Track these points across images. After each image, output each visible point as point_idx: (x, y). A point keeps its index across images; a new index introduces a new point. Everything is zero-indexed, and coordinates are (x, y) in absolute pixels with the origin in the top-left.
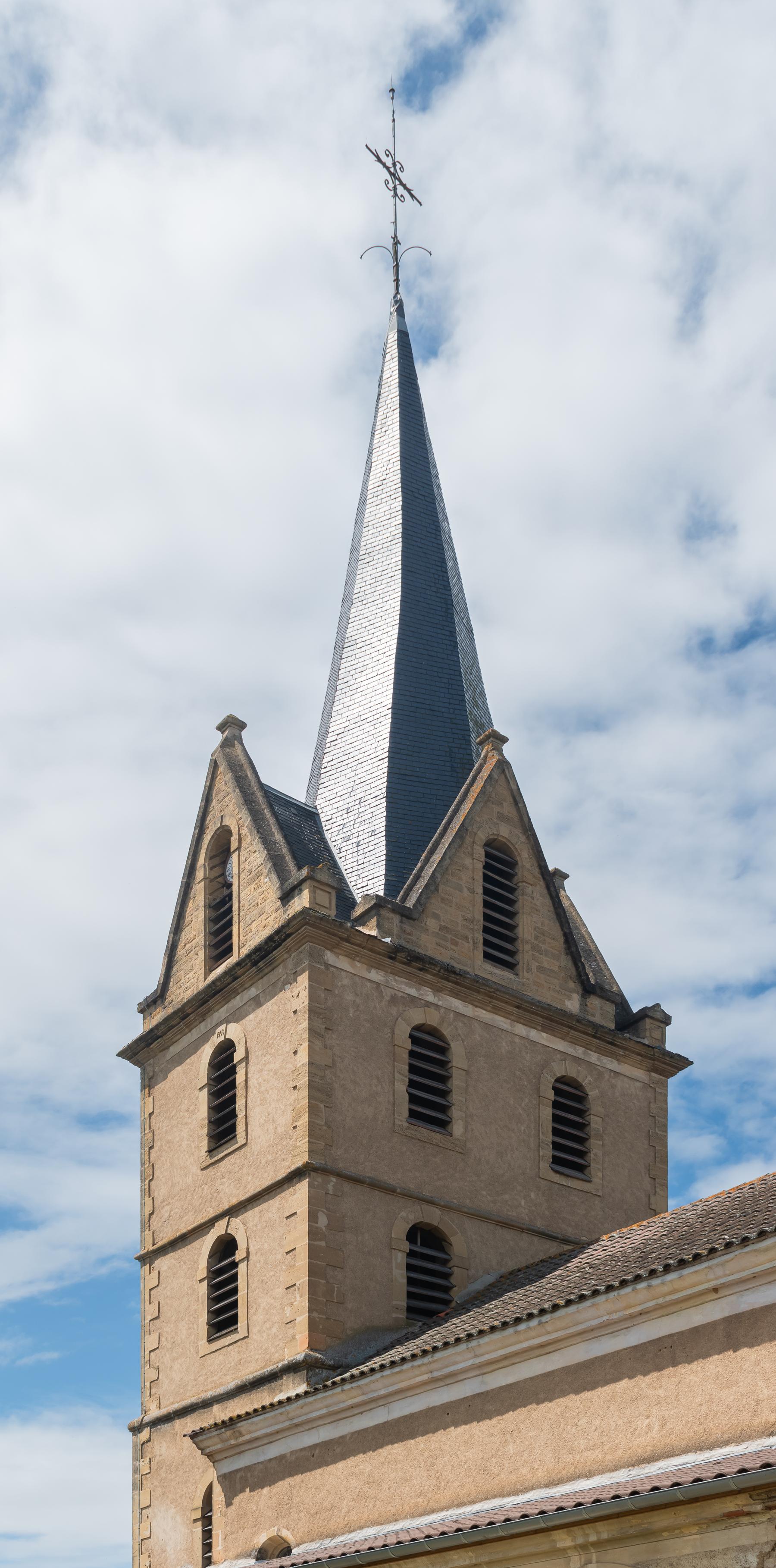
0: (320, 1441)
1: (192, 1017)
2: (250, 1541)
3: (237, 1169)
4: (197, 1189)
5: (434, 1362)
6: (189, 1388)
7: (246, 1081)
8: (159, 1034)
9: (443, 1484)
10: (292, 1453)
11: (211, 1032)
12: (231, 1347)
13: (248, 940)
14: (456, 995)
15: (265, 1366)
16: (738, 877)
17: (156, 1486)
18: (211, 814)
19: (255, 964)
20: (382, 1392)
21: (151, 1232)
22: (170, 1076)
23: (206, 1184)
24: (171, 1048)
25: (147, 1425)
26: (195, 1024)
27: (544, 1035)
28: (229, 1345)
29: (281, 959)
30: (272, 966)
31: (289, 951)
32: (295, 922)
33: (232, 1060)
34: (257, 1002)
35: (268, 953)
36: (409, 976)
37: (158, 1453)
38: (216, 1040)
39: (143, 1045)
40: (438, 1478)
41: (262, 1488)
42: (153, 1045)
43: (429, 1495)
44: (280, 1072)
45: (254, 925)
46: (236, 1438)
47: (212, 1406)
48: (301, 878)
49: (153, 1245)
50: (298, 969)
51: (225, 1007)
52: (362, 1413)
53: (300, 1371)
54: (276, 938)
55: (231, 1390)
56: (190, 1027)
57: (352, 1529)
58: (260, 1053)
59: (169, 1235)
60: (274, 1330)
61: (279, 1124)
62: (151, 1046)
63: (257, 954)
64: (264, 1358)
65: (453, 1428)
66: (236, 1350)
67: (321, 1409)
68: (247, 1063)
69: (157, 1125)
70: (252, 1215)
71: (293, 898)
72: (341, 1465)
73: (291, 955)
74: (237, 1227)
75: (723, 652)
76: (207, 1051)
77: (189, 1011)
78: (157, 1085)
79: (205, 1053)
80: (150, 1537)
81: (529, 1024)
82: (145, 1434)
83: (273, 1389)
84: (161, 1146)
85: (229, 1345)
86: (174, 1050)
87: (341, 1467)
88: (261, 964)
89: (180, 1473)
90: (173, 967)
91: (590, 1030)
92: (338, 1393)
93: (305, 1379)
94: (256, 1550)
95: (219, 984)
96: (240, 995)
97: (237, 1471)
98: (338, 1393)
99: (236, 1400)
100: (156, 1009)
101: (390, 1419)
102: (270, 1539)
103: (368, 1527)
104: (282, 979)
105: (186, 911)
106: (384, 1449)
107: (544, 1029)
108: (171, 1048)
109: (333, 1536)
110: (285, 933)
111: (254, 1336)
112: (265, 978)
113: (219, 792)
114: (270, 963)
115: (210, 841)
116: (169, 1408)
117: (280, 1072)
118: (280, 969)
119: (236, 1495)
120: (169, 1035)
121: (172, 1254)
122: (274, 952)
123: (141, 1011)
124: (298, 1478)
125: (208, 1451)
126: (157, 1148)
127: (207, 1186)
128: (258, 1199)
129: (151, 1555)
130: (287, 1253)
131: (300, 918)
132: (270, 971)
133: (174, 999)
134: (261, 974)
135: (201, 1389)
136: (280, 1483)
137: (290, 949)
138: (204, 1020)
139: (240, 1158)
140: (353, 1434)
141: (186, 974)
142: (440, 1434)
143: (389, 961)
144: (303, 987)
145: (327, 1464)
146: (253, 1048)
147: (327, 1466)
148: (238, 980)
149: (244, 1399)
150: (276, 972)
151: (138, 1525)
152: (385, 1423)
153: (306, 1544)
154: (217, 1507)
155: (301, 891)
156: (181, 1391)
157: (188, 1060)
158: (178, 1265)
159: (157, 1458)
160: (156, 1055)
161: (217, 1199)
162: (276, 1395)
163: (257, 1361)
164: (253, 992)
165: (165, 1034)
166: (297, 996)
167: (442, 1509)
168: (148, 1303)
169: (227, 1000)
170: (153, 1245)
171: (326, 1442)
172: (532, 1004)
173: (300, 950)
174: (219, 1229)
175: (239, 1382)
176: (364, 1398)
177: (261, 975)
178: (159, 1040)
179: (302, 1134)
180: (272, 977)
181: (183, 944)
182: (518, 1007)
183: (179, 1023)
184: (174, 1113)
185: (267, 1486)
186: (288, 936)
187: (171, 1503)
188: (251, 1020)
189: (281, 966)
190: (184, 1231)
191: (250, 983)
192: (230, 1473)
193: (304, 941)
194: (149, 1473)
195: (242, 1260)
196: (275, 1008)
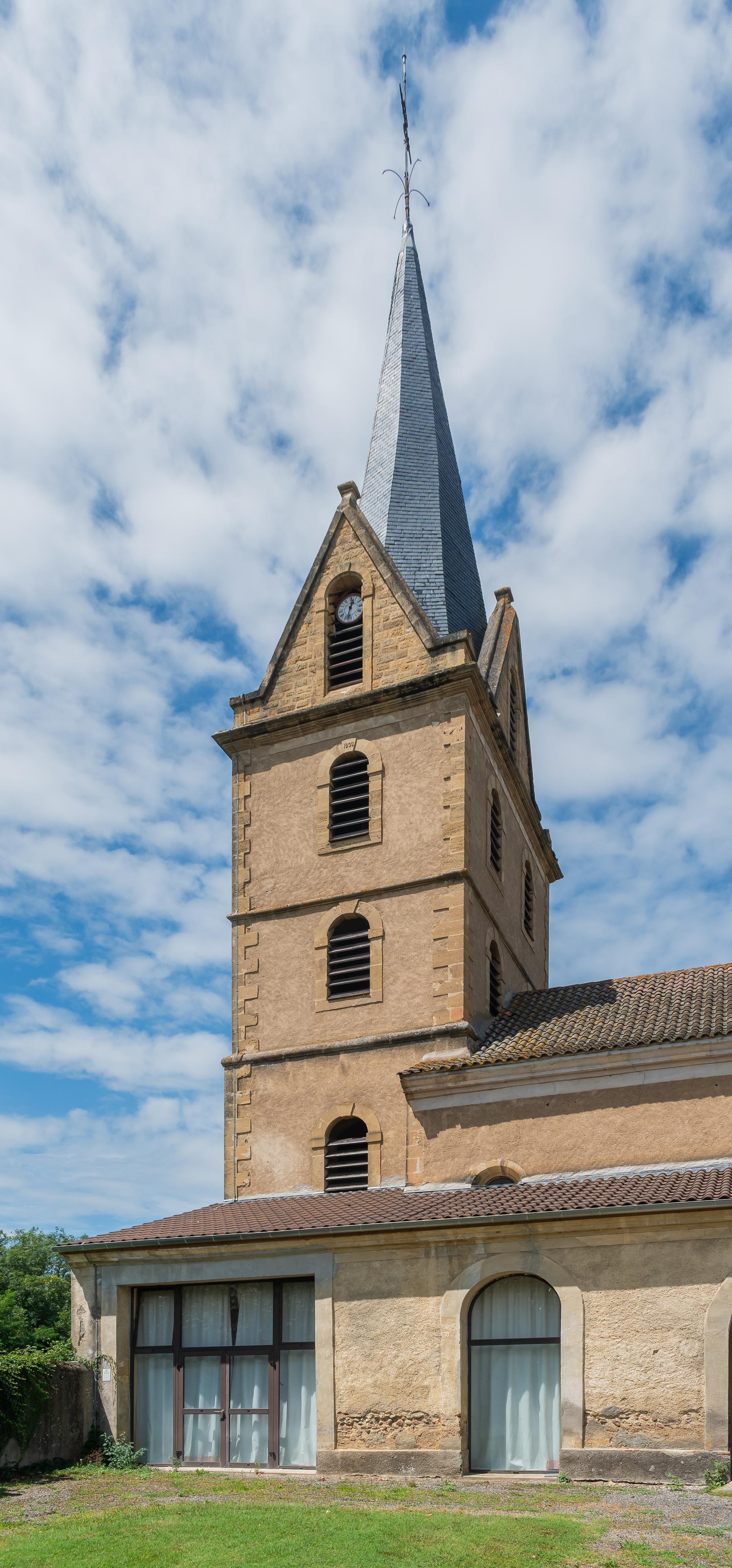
0: (557, 1093)
1: (313, 723)
2: (464, 1168)
3: (368, 862)
4: (312, 871)
5: (722, 1043)
6: (301, 1037)
7: (382, 790)
8: (268, 729)
9: (711, 1138)
10: (519, 1100)
11: (338, 741)
12: (358, 1008)
13: (384, 674)
15: (406, 1029)
17: (259, 1116)
18: (333, 557)
19: (402, 695)
20: (650, 1061)
21: (248, 898)
22: (275, 769)
23: (325, 868)
24: (276, 745)
25: (247, 1062)
26: (312, 730)
28: (356, 1006)
29: (429, 700)
30: (419, 702)
31: (442, 694)
32: (463, 672)
33: (366, 769)
34: (396, 729)
35: (420, 690)
37: (262, 1087)
38: (343, 748)
39: (247, 734)
40: (706, 1133)
41: (479, 1126)
42: (257, 737)
43: (695, 1146)
44: (426, 791)
45: (392, 664)
46: (456, 1082)
47: (339, 1054)
48: (459, 638)
49: (250, 910)
50: (452, 712)
51: (353, 724)
52: (611, 1076)
53: (459, 1037)
54: (437, 679)
55: (368, 1043)
56: (305, 732)
57: (600, 1166)
58: (400, 771)
59: (272, 904)
60: (417, 1000)
61: (425, 834)
62: (255, 738)
63: (410, 688)
64: (404, 1021)
65: (723, 1096)
66: (367, 1011)
67: (574, 1067)
68: (383, 776)
69: (256, 808)
70: (387, 904)
71: (444, 652)
72: (584, 1115)
73: (442, 698)
74: (366, 909)
75: (111, 605)
76: (328, 758)
77: (311, 718)
78: (255, 773)
79: (325, 758)
80: (250, 1159)
82: (244, 1070)
83: (423, 1048)
84: (261, 826)
85: (356, 1006)
86: (278, 747)
87: (584, 1117)
88: (408, 698)
89: (294, 1107)
90: (278, 676)
92: (603, 1057)
93: (465, 1043)
94: (472, 1177)
95: (357, 702)
96: (374, 718)
97: (442, 1110)
98: (603, 1057)
99: (371, 1052)
100: (253, 707)
101: (646, 1082)
102: (489, 1169)
103: (621, 1166)
104: (429, 716)
105: (298, 632)
106: (639, 1106)
108: (276, 745)
109: (576, 1170)
110: (448, 678)
111: (391, 1000)
112: (406, 711)
113: (343, 542)
114: (418, 699)
115: (332, 581)
116: (281, 1050)
117: (426, 791)
118: (427, 707)
119: (442, 1130)
120: (280, 732)
121: (276, 921)
122: (427, 691)
123: (234, 706)
124: (528, 1122)
125: (408, 1090)
126: (256, 827)
127: (326, 870)
128: (398, 890)
129: (251, 1174)
130: (435, 940)
131: (469, 670)
132: (414, 706)
133: (280, 704)
134: (404, 706)
135: (317, 1039)
136: (505, 1124)
137: (445, 693)
138: (324, 729)
139: (372, 853)
140: (600, 1091)
141: (297, 686)
142: (708, 1100)
144: (459, 727)
145: (567, 1113)
146: (390, 763)
147: (567, 1114)
148: (379, 705)
149: (382, 1052)
150: (421, 708)
151: (233, 1147)
152: (640, 1086)
153: (541, 1176)
154: (414, 1138)
155: (454, 650)
156: (290, 1038)
157: (301, 760)
158: (285, 931)
159: (260, 1092)
160: (255, 747)
161: (341, 883)
162: (425, 1053)
163: (394, 1023)
164: (391, 718)
165: (275, 730)
166: (451, 733)
167: (712, 1158)
168: (243, 958)
169: (357, 719)
170: (250, 910)
171: (564, 1095)
173: (455, 696)
174: (346, 908)
175: (379, 1038)
176: (628, 1063)
177: (404, 706)
178: (266, 735)
179: (456, 846)
180: (417, 711)
181: (293, 659)
183: (297, 725)
184: (279, 801)
185: (486, 1124)
186: (449, 681)
187: (280, 1132)
188: (388, 742)
189: (429, 704)
190: (299, 903)
191: (389, 711)
192: (438, 1110)
193: (461, 690)
194: (250, 1104)
195: (377, 938)
196: (419, 738)
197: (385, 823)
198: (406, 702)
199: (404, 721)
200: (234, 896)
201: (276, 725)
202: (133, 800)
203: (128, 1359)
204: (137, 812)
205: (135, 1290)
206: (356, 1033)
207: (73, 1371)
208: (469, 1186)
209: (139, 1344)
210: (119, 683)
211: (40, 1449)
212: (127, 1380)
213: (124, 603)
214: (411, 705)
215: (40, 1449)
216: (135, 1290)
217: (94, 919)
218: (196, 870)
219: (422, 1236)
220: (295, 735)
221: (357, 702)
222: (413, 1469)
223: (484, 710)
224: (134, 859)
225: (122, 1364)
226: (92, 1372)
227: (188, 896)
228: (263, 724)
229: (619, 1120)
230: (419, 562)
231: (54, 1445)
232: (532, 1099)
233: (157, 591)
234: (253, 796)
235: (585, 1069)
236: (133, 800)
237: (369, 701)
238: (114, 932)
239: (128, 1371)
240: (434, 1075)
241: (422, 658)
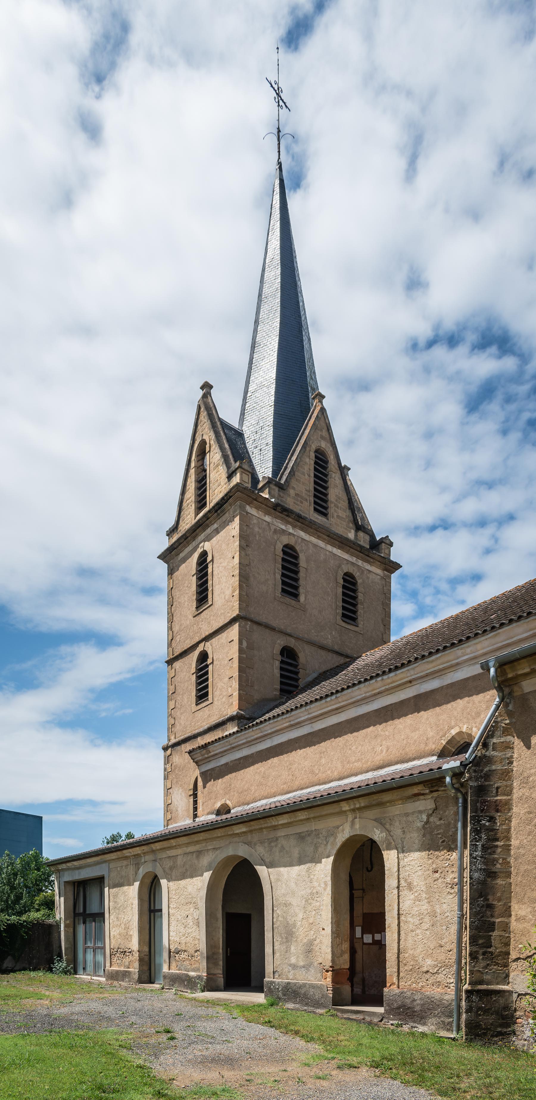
7: (212, 572)
14: (302, 529)
15: (220, 718)
16: (425, 469)
20: (269, 731)
27: (339, 551)
28: (205, 707)
30: (224, 512)
34: (217, 531)
35: (222, 506)
36: (282, 519)
39: (168, 552)
41: (219, 779)
56: (188, 544)
68: (213, 563)
81: (333, 545)
86: (182, 555)
88: (219, 511)
91: (359, 549)
101: (272, 745)
102: (222, 805)
107: (340, 548)
109: (248, 804)
111: (215, 703)
120: (180, 547)
125: (196, 760)
134: (219, 517)
138: (194, 540)
140: (257, 752)
143: (273, 511)
164: (215, 526)
172: (335, 535)
177: (219, 517)
180: (224, 518)
182: (328, 536)
186: (231, 497)
190: (186, 648)
192: (205, 771)
197: (214, 591)
198: (218, 515)
199: (220, 526)
200: (168, 648)
201: (177, 544)
202: (444, 489)
203: (72, 920)
204: (447, 498)
205: (76, 884)
206: (205, 723)
207: (47, 925)
208: (214, 816)
209: (77, 912)
210: (429, 407)
211: (26, 962)
212: (72, 930)
213: (431, 344)
214: (221, 515)
215: (26, 962)
216: (76, 884)
217: (423, 586)
218: (489, 530)
219: (126, 853)
220: (185, 547)
221: (201, 521)
222: (127, 979)
223: (261, 503)
224: (447, 533)
225: (68, 922)
226: (58, 926)
227: (488, 551)
228: (172, 545)
229: (263, 769)
230: (263, 401)
231: (34, 961)
232: (235, 760)
233: (449, 325)
234: (174, 587)
235: (249, 739)
236: (444, 489)
237: (205, 519)
238: (438, 592)
239: (72, 925)
240: (199, 751)
241: (225, 484)
